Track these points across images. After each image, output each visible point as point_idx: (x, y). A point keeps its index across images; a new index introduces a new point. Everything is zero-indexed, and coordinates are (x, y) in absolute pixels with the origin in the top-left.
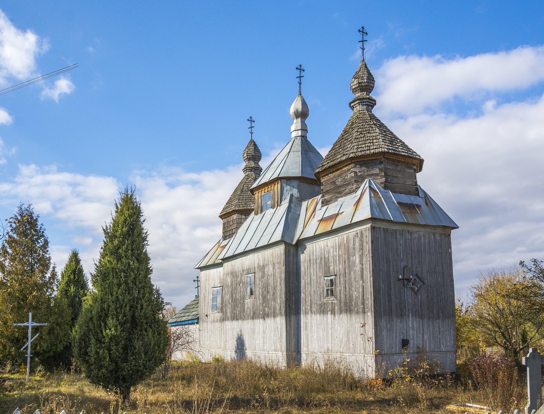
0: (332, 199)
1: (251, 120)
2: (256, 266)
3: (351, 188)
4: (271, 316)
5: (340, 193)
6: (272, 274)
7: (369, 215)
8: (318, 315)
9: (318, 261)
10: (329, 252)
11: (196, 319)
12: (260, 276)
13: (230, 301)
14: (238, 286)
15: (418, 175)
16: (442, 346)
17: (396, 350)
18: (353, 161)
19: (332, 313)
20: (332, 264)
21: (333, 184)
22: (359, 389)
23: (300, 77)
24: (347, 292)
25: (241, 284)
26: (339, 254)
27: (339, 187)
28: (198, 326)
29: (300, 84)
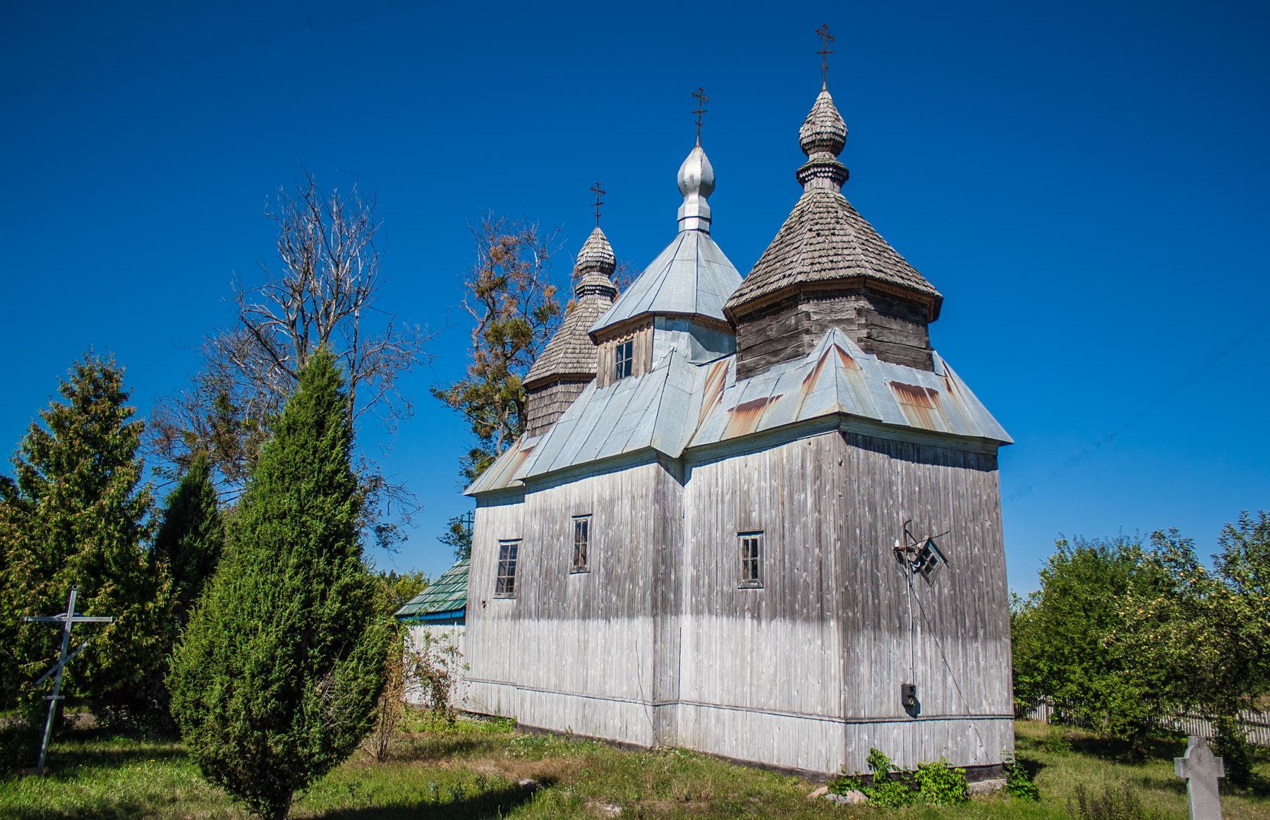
5: (775, 353)
8: (725, 619)
13: (537, 573)
16: (984, 702)
19: (753, 617)
20: (757, 506)
24: (787, 570)
27: (770, 341)
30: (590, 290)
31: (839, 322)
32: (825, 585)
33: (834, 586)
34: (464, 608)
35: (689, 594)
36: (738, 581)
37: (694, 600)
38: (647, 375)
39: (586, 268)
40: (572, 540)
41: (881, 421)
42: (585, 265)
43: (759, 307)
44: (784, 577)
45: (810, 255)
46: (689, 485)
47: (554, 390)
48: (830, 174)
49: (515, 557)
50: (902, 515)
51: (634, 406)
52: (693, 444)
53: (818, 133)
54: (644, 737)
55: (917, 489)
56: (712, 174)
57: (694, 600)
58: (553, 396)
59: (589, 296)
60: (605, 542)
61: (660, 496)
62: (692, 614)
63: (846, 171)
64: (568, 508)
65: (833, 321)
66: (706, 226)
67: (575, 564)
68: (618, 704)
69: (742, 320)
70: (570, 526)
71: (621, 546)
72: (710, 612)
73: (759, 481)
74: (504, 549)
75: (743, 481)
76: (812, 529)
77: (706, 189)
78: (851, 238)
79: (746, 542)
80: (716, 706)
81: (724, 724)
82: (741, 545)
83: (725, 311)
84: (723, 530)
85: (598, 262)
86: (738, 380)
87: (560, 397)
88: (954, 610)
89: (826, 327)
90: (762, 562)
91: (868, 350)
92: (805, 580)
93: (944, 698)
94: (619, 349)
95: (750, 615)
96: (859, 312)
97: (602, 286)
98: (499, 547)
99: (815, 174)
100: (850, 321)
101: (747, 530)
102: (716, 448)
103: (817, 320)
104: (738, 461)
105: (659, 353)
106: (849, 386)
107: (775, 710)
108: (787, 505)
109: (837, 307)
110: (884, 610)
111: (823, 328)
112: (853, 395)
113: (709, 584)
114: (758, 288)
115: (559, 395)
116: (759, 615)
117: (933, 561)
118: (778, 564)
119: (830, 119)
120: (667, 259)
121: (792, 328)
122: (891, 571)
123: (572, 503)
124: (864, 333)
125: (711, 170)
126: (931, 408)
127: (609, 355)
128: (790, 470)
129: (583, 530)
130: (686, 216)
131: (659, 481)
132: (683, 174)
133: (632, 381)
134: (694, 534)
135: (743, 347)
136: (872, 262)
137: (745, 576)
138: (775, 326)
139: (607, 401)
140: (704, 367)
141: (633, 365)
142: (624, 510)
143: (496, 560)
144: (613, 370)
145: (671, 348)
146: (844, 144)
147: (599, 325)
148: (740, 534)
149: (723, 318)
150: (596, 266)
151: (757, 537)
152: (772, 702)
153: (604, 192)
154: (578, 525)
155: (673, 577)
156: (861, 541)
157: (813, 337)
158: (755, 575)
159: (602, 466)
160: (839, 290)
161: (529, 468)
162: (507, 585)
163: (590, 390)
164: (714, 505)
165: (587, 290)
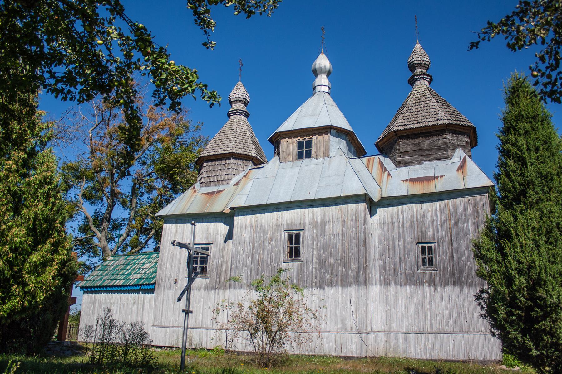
2: (307, 221)
3: (444, 154)
4: (337, 285)
5: (426, 156)
6: (340, 233)
8: (408, 287)
9: (407, 225)
10: (424, 216)
13: (248, 262)
14: (267, 244)
19: (430, 285)
20: (431, 230)
21: (416, 146)
30: (240, 113)
31: (461, 146)
34: (155, 283)
37: (382, 278)
39: (237, 101)
43: (416, 132)
44: (453, 265)
46: (375, 218)
47: (228, 161)
53: (423, 60)
57: (382, 278)
59: (239, 116)
62: (381, 285)
68: (333, 336)
71: (333, 248)
72: (396, 283)
75: (419, 217)
79: (423, 249)
80: (403, 333)
82: (420, 250)
84: (404, 241)
85: (244, 99)
90: (436, 257)
92: (469, 266)
95: (427, 285)
99: (423, 78)
101: (423, 241)
102: (399, 199)
103: (453, 143)
104: (415, 207)
107: (451, 332)
108: (453, 229)
109: (460, 139)
113: (395, 270)
116: (434, 284)
121: (439, 145)
134: (380, 242)
137: (424, 263)
138: (426, 143)
148: (418, 243)
150: (242, 101)
151: (432, 245)
159: (314, 203)
160: (461, 131)
164: (396, 229)
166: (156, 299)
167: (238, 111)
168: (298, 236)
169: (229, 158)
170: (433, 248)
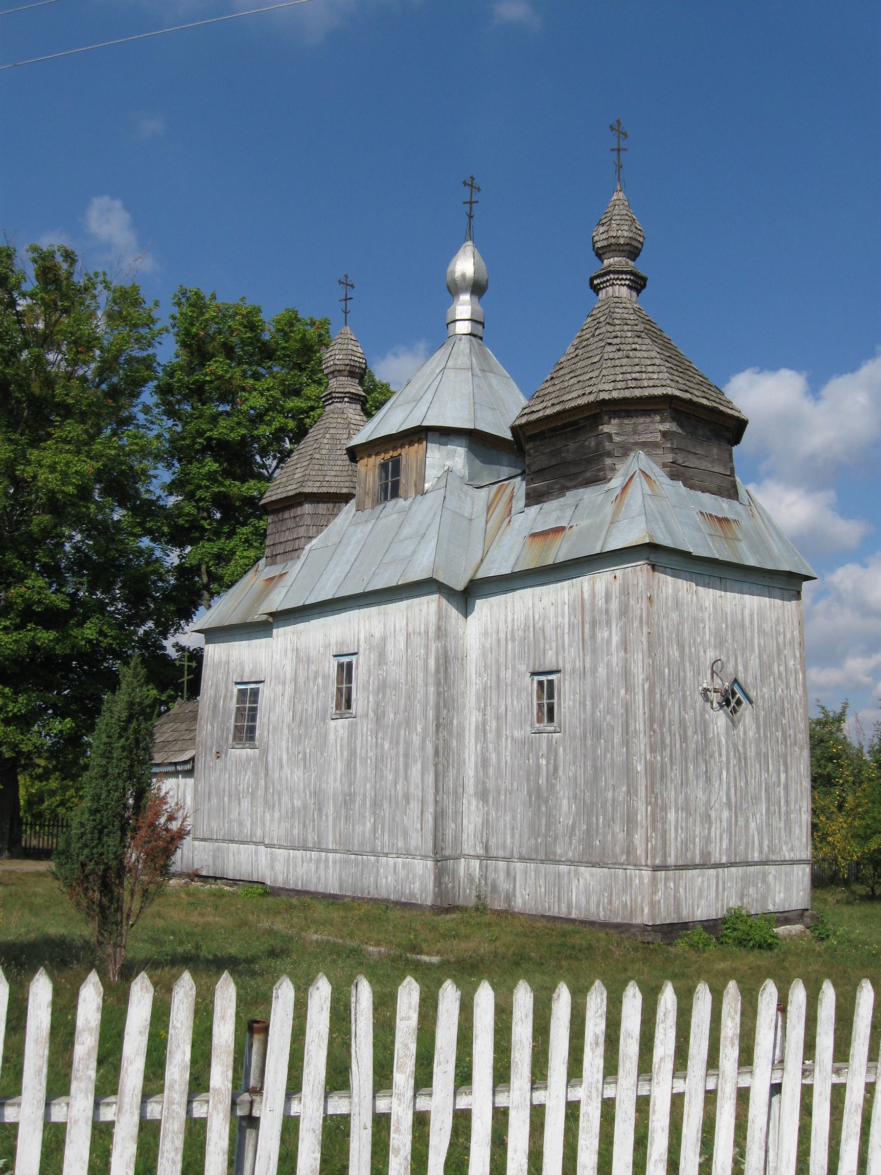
0: (552, 489)
1: (347, 284)
7: (645, 537)
11: (190, 760)
12: (372, 663)
15: (735, 449)
16: (784, 848)
17: (693, 858)
18: (604, 409)
22: (577, 947)
23: (471, 203)
24: (589, 712)
25: (320, 680)
26: (569, 622)
28: (190, 781)
29: (471, 217)
30: (338, 398)
31: (644, 445)
32: (631, 728)
33: (642, 728)
35: (473, 741)
36: (532, 725)
38: (419, 498)
39: (333, 372)
40: (333, 683)
41: (690, 553)
42: (331, 369)
45: (612, 371)
47: (299, 511)
48: (627, 282)
49: (256, 702)
50: (711, 655)
51: (406, 531)
52: (479, 575)
54: (424, 895)
55: (724, 626)
56: (486, 273)
57: (478, 747)
58: (298, 519)
60: (374, 683)
61: (441, 632)
63: (644, 279)
64: (327, 646)
65: (636, 444)
66: (479, 330)
67: (337, 709)
69: (532, 438)
70: (331, 667)
73: (556, 617)
74: (242, 693)
76: (617, 669)
77: (478, 289)
78: (654, 354)
79: (540, 683)
81: (515, 878)
83: (514, 429)
86: (527, 505)
87: (307, 520)
88: (758, 754)
89: (631, 450)
90: (559, 705)
91: (673, 476)
93: (747, 844)
94: (384, 466)
96: (664, 434)
97: (352, 393)
98: (235, 691)
100: (655, 445)
105: (432, 475)
106: (658, 516)
110: (691, 754)
111: (625, 451)
112: (661, 525)
114: (553, 405)
115: (306, 517)
117: (739, 703)
118: (577, 706)
119: (627, 223)
120: (437, 366)
122: (698, 714)
123: (333, 641)
124: (669, 458)
125: (485, 268)
126: (738, 540)
127: (370, 474)
128: (593, 603)
129: (346, 672)
130: (457, 318)
131: (441, 616)
132: (453, 272)
133: (401, 502)
135: (533, 469)
136: (678, 382)
137: (540, 720)
139: (370, 525)
140: (484, 489)
141: (401, 485)
142: (396, 648)
143: (233, 705)
144: (376, 491)
145: (446, 468)
146: (640, 250)
147: (359, 439)
149: (508, 435)
152: (570, 854)
153: (352, 286)
154: (340, 666)
155: (455, 722)
156: (669, 680)
157: (615, 461)
158: (551, 719)
161: (278, 601)
162: (247, 733)
163: (347, 513)
165: (336, 398)
166: (196, 785)
167: (334, 395)
168: (255, 693)
169: (301, 504)
170: (556, 683)
